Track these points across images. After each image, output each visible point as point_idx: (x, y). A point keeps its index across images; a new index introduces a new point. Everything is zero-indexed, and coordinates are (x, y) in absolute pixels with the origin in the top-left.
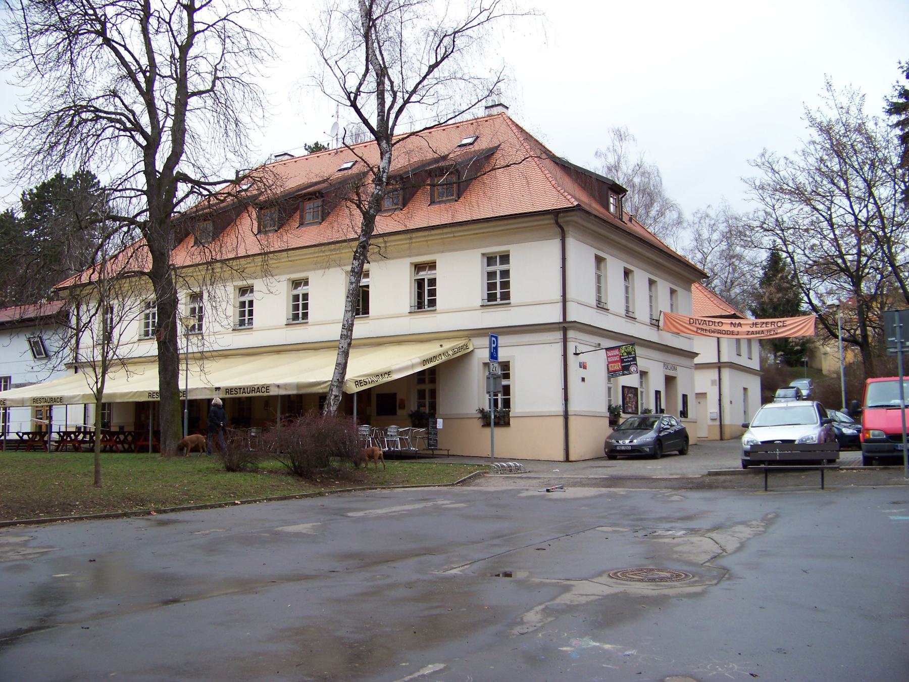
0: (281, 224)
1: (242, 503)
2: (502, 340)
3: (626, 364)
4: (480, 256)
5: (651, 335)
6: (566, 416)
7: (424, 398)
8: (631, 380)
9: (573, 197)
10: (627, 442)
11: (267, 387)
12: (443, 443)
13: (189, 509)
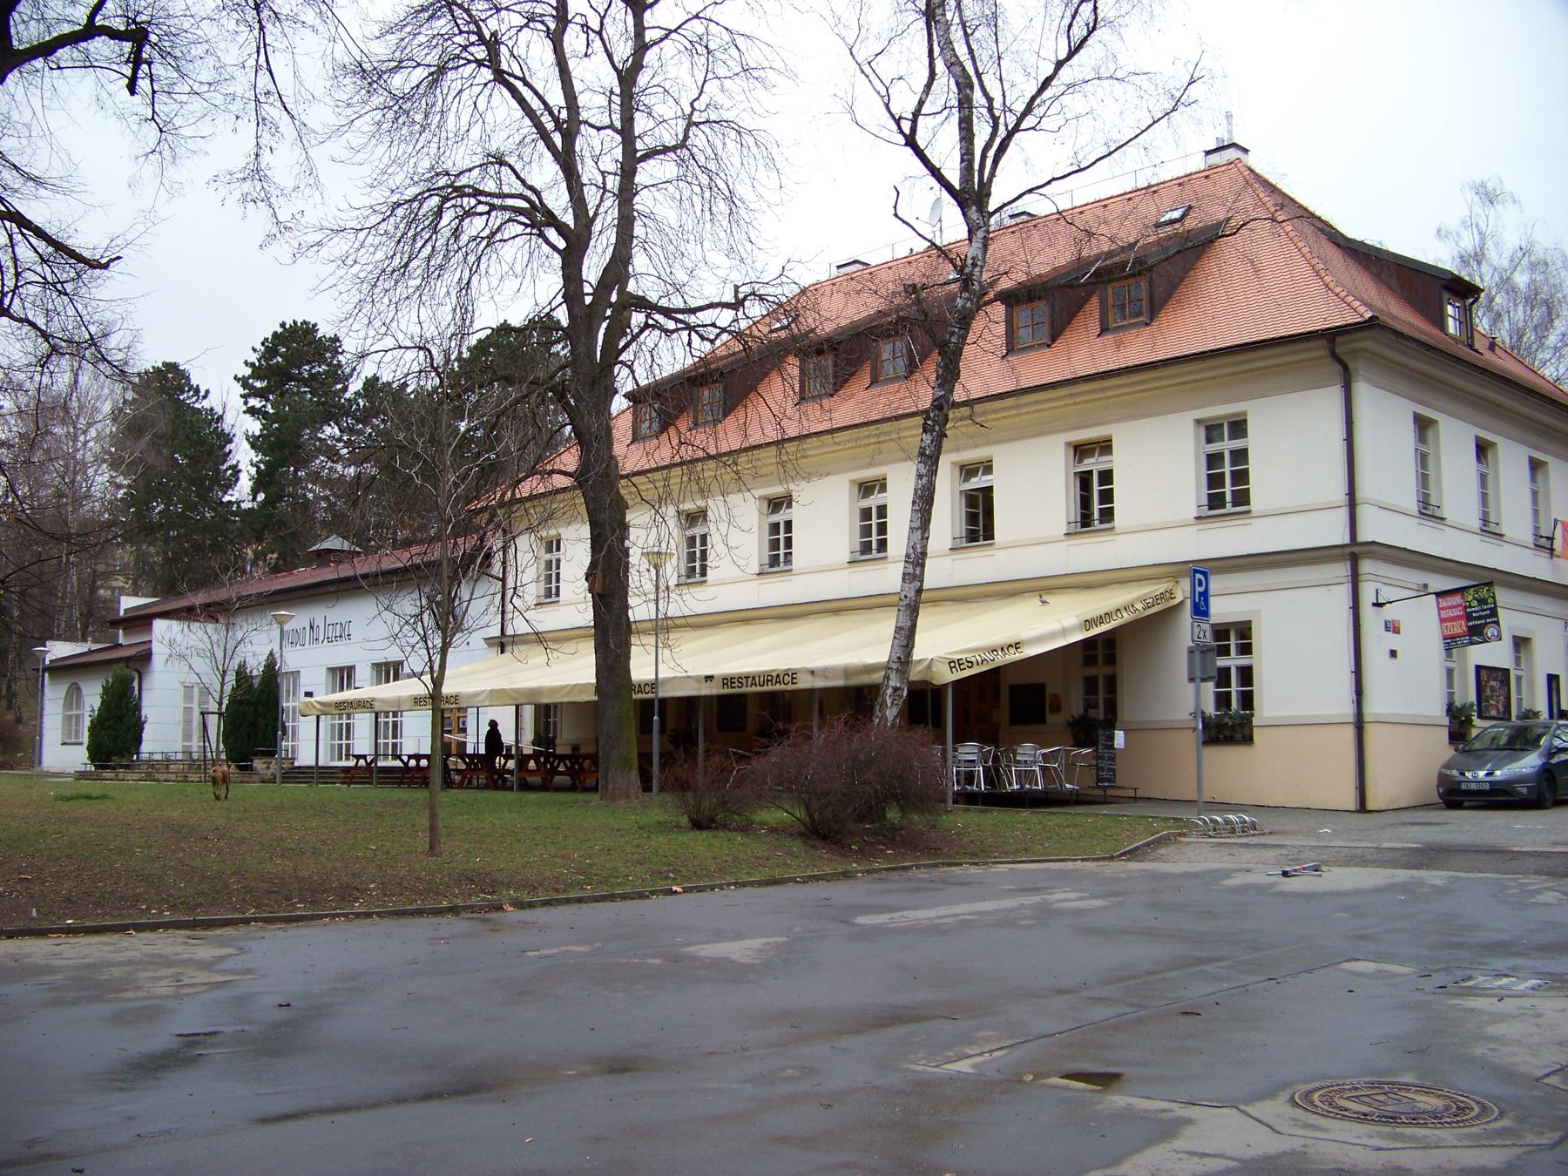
0: (840, 381)
1: (686, 890)
2: (1216, 583)
3: (1478, 625)
4: (1191, 424)
5: (1538, 567)
6: (1359, 724)
7: (1096, 692)
8: (1494, 654)
9: (1365, 303)
10: (1481, 774)
11: (792, 675)
12: (1126, 777)
13: (580, 900)
